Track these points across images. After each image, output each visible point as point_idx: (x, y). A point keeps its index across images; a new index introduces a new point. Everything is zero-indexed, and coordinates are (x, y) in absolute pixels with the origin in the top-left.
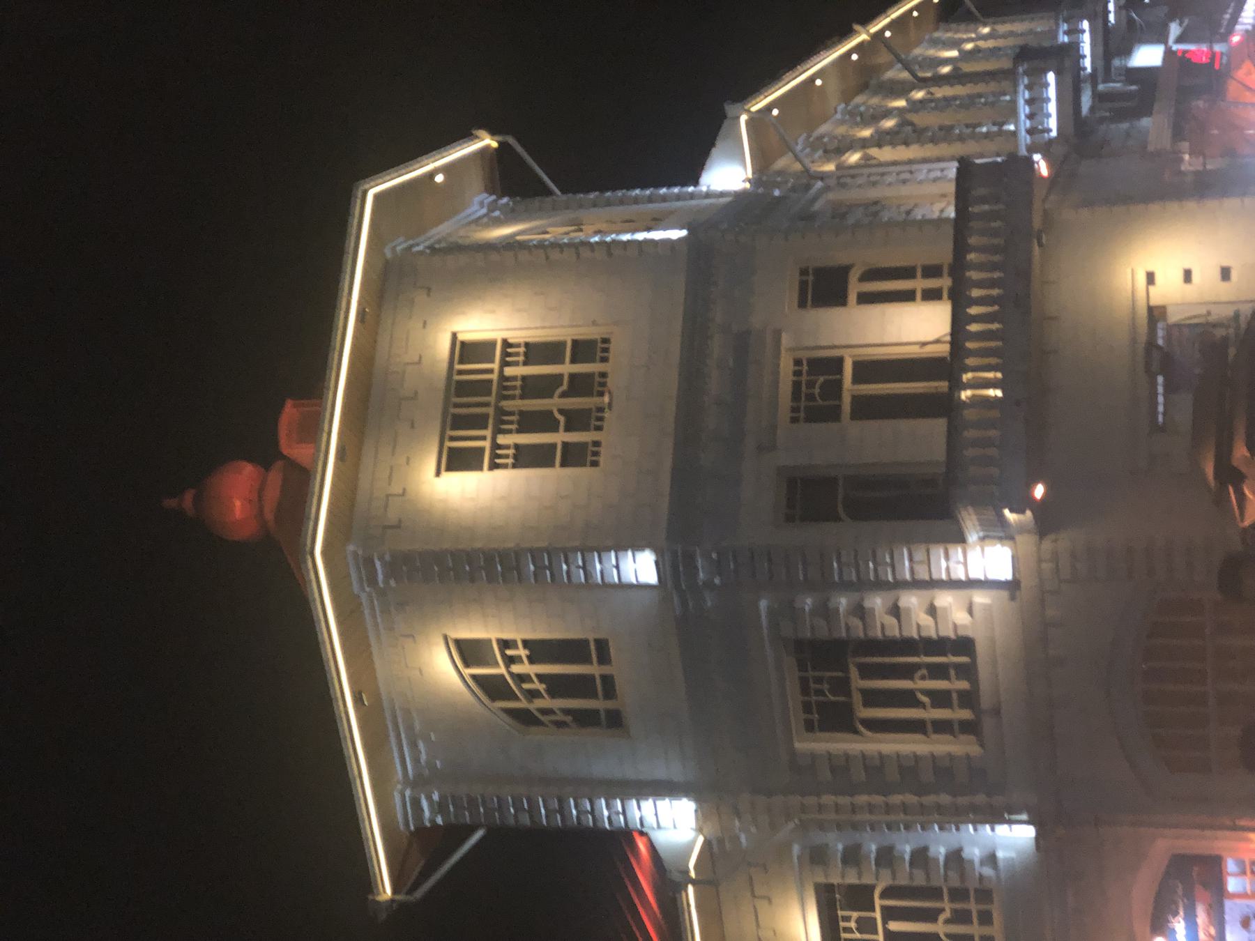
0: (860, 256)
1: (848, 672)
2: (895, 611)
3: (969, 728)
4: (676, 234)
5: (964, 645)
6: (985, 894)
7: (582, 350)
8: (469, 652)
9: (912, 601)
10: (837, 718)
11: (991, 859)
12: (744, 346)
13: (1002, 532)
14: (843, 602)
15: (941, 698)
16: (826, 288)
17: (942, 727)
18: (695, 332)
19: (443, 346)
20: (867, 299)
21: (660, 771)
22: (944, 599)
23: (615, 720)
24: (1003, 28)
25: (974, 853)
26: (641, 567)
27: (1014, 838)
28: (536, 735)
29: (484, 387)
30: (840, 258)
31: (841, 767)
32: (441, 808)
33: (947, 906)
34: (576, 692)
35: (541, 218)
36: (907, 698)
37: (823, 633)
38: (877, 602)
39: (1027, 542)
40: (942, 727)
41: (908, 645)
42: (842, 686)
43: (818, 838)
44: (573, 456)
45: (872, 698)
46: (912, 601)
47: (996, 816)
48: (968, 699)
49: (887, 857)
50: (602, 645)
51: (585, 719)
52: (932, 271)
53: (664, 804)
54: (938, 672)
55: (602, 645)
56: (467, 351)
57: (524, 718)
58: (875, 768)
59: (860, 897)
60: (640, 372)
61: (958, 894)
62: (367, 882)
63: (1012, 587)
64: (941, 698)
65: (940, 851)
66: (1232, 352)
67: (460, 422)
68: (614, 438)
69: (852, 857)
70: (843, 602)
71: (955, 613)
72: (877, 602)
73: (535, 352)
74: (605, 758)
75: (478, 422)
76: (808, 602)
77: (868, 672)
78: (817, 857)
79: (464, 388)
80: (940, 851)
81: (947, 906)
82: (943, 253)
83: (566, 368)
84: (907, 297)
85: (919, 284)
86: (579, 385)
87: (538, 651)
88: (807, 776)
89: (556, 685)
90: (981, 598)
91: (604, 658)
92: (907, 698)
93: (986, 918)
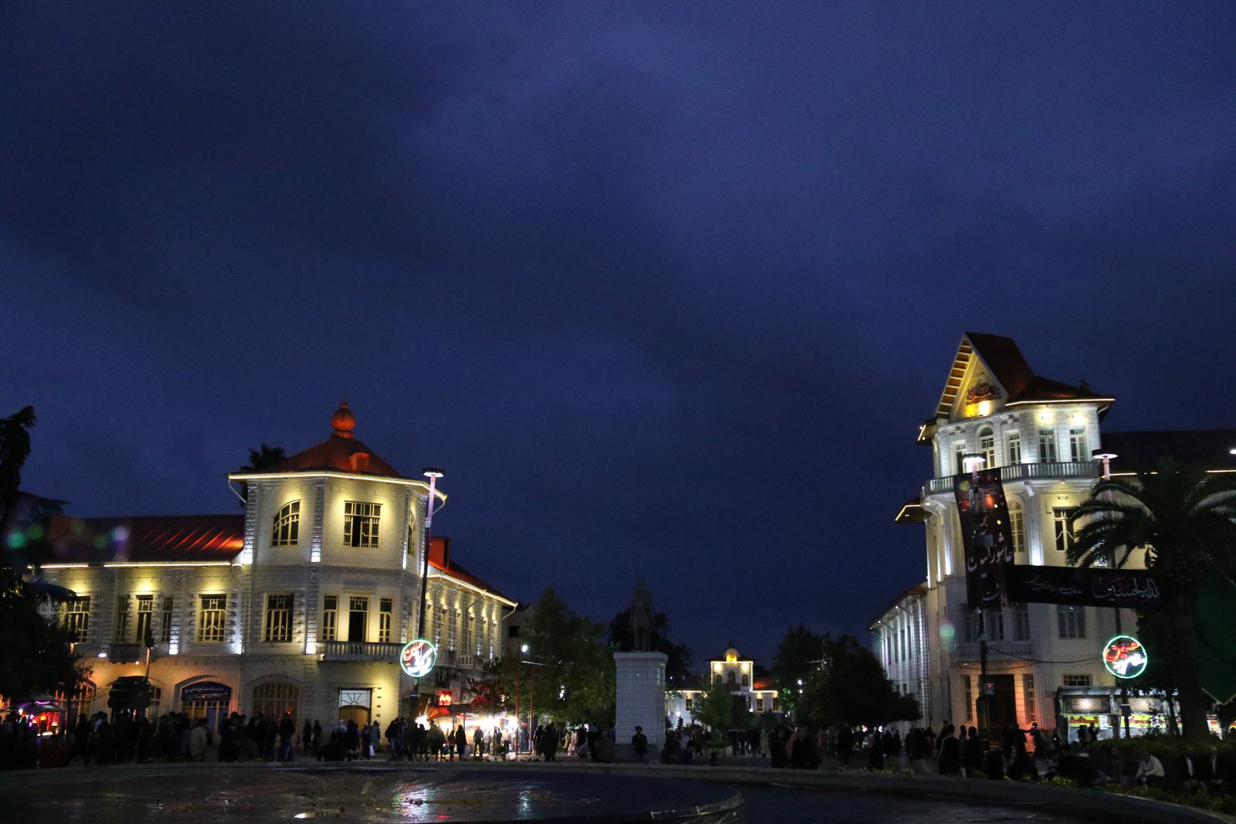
0: (394, 614)
1: (283, 609)
2: (300, 623)
3: (268, 639)
4: (404, 566)
5: (290, 639)
6: (221, 639)
7: (375, 540)
8: (296, 506)
9: (302, 627)
10: (272, 603)
11: (232, 642)
12: (373, 584)
13: (319, 652)
14: (303, 609)
15: (276, 632)
16: (386, 606)
17: (268, 632)
18: (377, 572)
19: (378, 501)
20: (382, 616)
21: (260, 555)
22: (302, 636)
23: (275, 544)
24: (496, 629)
25: (234, 637)
26: (316, 558)
27: (237, 648)
28: (272, 520)
29: (367, 513)
30: (393, 610)
31: (259, 604)
32: (253, 491)
33: (218, 629)
34: (284, 535)
35: (418, 514)
36: (276, 623)
37: (296, 603)
38: (303, 618)
39: (316, 658)
40: (268, 632)
41: (291, 625)
42: (281, 607)
43: (240, 596)
44: (347, 538)
45: (277, 615)
46: (302, 627)
47: (244, 644)
48: (275, 639)
49: (233, 614)
50: (295, 543)
51: (275, 535)
52: (388, 634)
53: (251, 556)
54: (283, 632)
55: (295, 543)
56: (378, 508)
57: (277, 518)
58: (258, 614)
59: (222, 605)
60: (365, 556)
61: (222, 632)
62: (233, 474)
63: (305, 653)
64: (276, 632)
65: (234, 628)
66: (38, 762)
67: (358, 506)
68: (351, 550)
69: (234, 605)
70: (303, 609)
71: (298, 638)
72: (303, 618)
73: (376, 528)
74: (266, 538)
75: (358, 512)
76: (304, 600)
77: (284, 614)
78: (234, 596)
79: (367, 507)
80: (234, 628)
81: (218, 629)
82: (392, 640)
83: (370, 536)
84: (382, 627)
85: (385, 630)
86: (366, 540)
87: (295, 525)
88: (256, 594)
89: (285, 529)
90: (302, 645)
91: (292, 543)
92: (276, 623)
93: (215, 638)
